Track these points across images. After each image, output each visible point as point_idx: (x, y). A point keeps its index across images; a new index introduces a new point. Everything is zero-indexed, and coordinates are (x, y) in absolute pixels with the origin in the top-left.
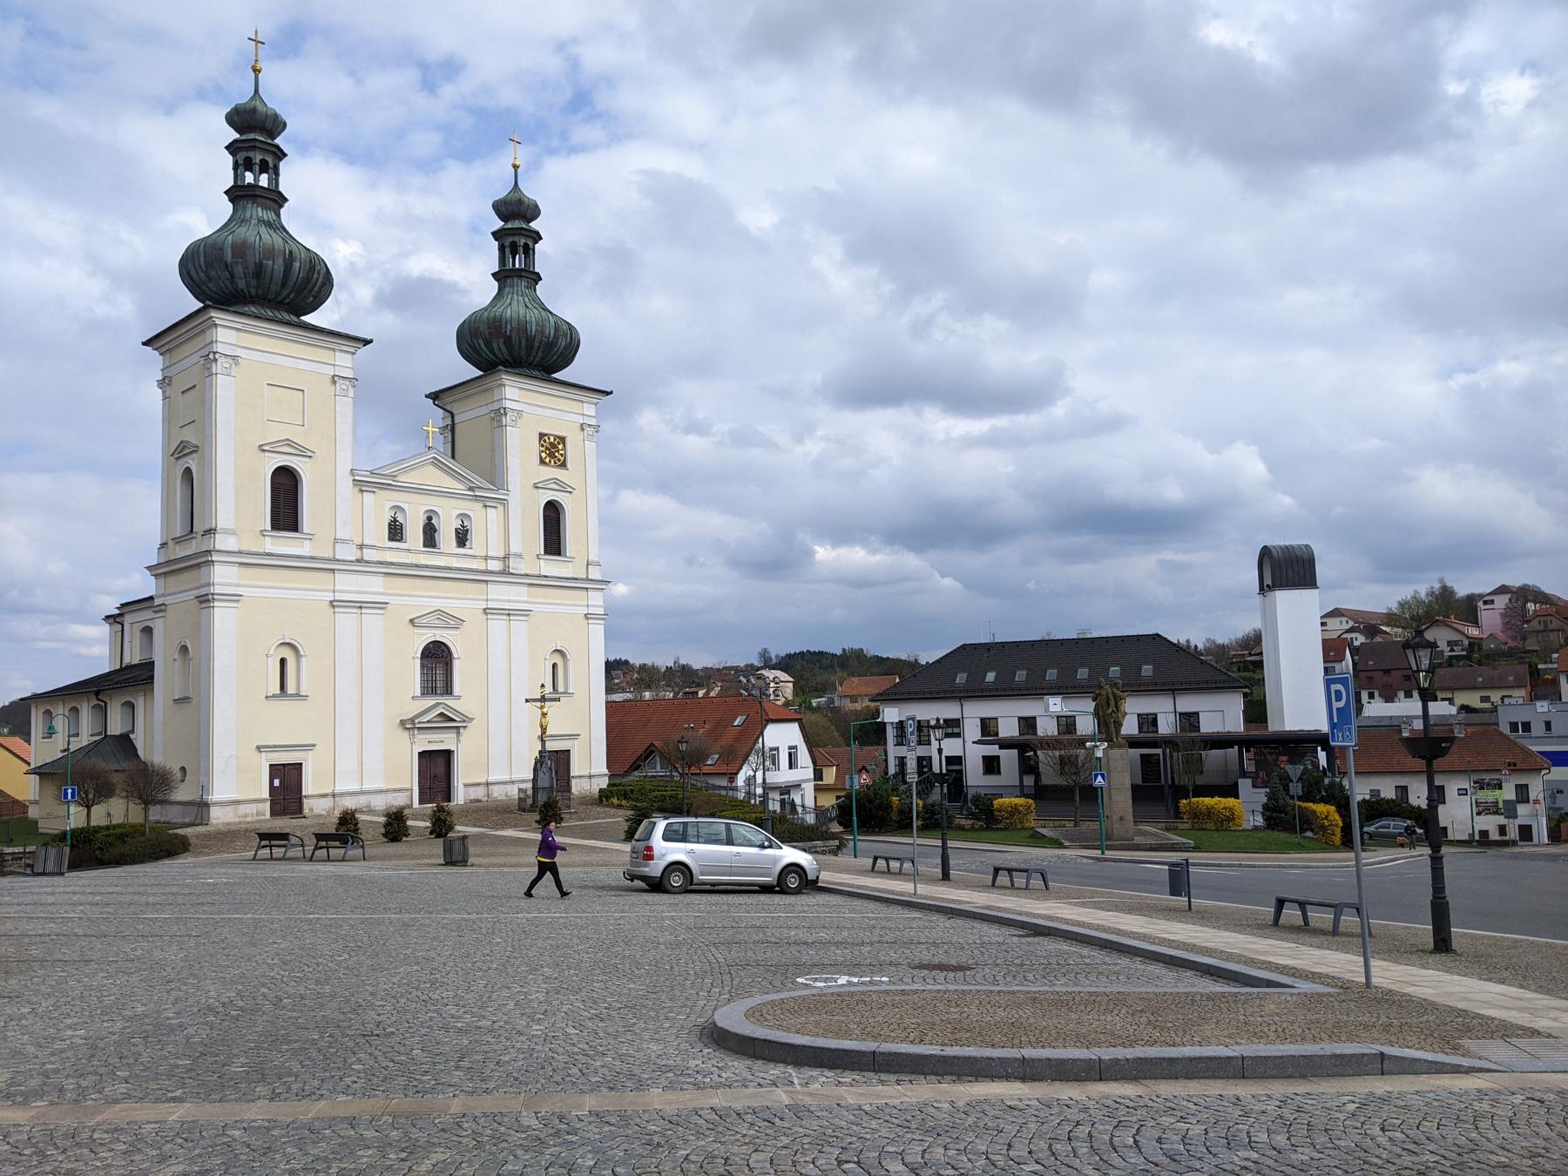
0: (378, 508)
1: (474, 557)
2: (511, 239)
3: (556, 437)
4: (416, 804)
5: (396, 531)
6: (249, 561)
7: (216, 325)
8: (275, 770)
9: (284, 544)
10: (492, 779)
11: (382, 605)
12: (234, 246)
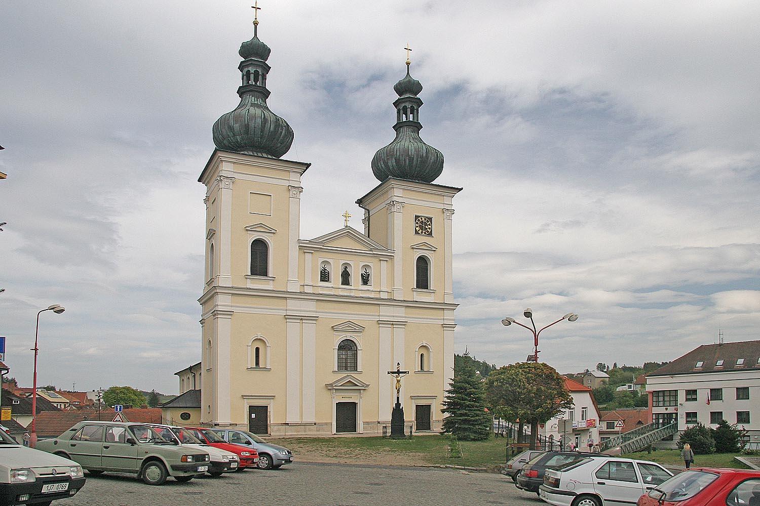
0: (314, 263)
2: (403, 105)
3: (426, 218)
5: (325, 276)
6: (236, 292)
8: (252, 409)
9: (259, 284)
11: (315, 318)
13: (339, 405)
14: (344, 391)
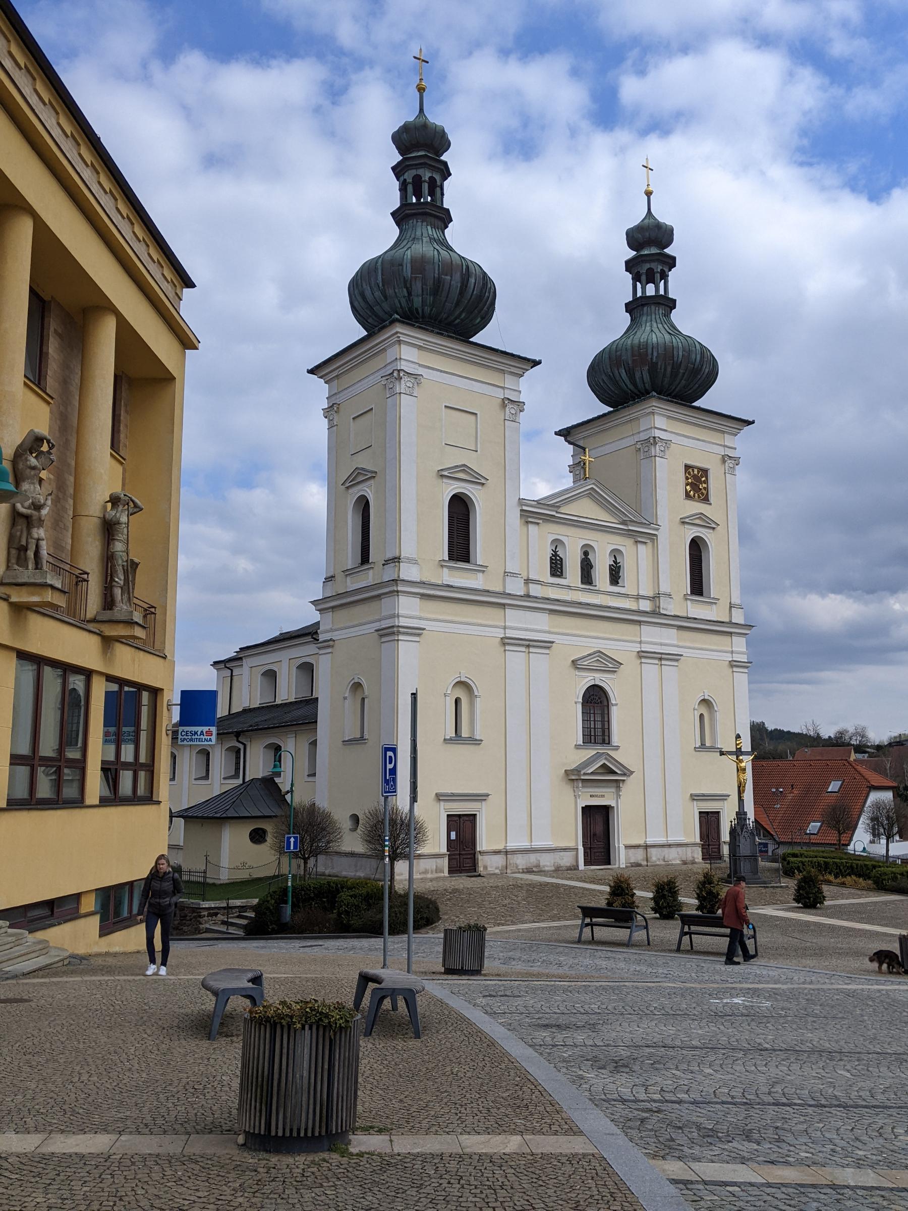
1: (627, 596)
2: (648, 266)
4: (581, 866)
5: (557, 567)
6: (431, 593)
7: (399, 342)
10: (650, 840)
12: (413, 261)
13: (587, 810)
14: (595, 784)
